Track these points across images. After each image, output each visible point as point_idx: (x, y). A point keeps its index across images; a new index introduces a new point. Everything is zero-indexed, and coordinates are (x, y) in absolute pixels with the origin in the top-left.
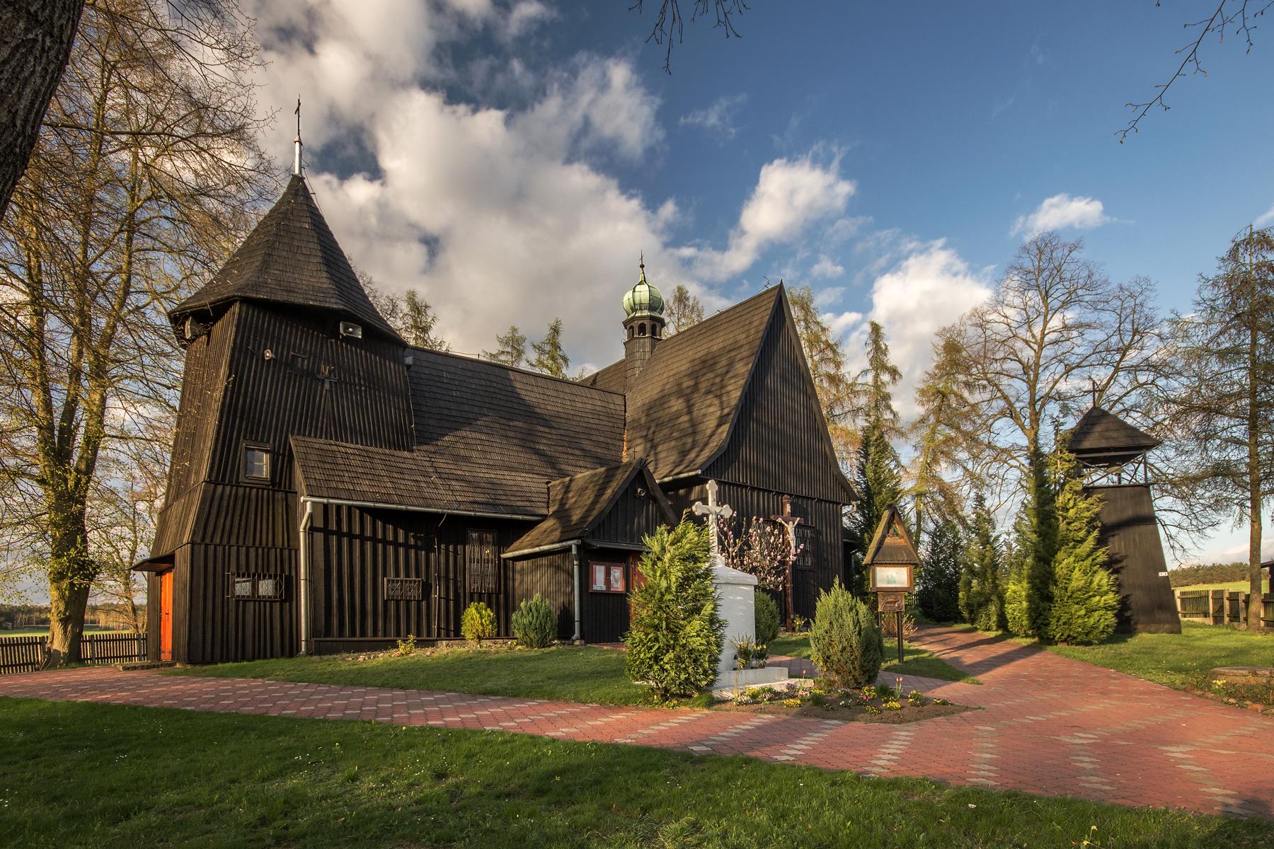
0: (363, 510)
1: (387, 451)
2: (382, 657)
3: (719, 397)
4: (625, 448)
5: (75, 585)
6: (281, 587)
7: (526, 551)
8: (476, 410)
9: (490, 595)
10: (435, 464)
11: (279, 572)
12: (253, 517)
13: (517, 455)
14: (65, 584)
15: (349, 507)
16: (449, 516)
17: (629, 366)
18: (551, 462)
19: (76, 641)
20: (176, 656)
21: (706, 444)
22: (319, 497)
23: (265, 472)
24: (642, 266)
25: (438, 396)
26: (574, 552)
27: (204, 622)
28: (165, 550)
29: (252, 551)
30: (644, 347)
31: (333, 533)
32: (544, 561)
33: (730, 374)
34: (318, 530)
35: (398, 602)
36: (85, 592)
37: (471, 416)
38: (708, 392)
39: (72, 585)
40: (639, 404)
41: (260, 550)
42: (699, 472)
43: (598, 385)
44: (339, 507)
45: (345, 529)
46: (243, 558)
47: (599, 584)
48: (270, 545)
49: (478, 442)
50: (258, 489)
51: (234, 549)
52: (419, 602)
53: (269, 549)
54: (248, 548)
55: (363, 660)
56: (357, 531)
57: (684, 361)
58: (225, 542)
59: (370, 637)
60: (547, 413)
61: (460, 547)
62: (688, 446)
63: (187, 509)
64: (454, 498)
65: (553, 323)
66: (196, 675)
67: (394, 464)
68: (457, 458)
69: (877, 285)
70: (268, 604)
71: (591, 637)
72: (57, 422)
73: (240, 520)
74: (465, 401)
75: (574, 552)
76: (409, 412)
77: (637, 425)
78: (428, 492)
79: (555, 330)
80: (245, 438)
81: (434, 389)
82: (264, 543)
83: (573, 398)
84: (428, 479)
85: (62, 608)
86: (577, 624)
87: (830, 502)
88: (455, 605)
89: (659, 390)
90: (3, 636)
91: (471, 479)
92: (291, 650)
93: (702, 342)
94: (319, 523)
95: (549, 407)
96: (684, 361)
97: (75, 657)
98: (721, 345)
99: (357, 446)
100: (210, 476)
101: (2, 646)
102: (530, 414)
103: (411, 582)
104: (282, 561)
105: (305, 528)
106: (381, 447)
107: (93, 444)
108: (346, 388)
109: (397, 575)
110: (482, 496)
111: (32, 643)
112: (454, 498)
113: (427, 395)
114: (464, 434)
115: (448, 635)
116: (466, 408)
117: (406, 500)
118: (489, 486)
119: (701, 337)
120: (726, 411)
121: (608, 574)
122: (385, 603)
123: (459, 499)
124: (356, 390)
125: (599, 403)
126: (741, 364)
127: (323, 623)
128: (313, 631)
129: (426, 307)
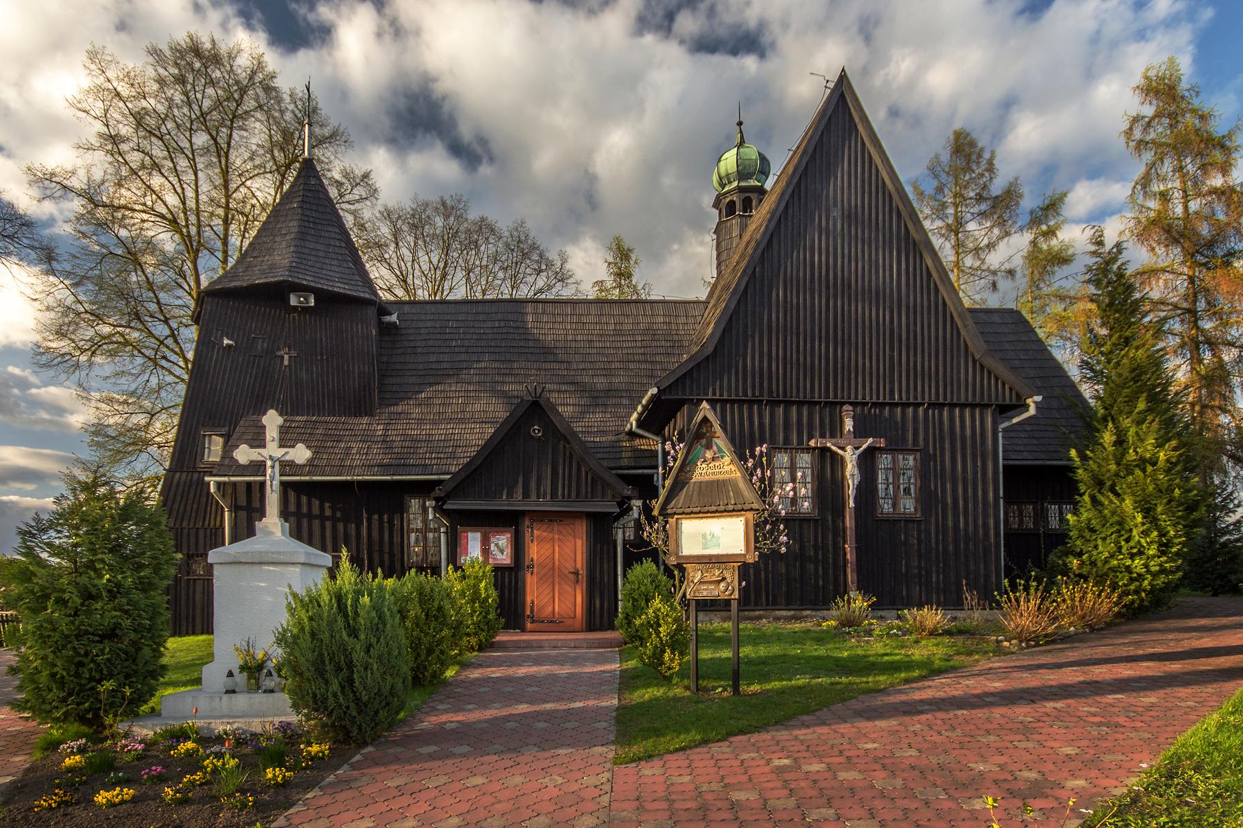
22: (220, 476)
24: (740, 124)
69: (682, 11)
82: (212, 524)
90: (4, 613)
101: (3, 622)
116: (433, 358)
121: (1021, 522)
129: (629, 250)
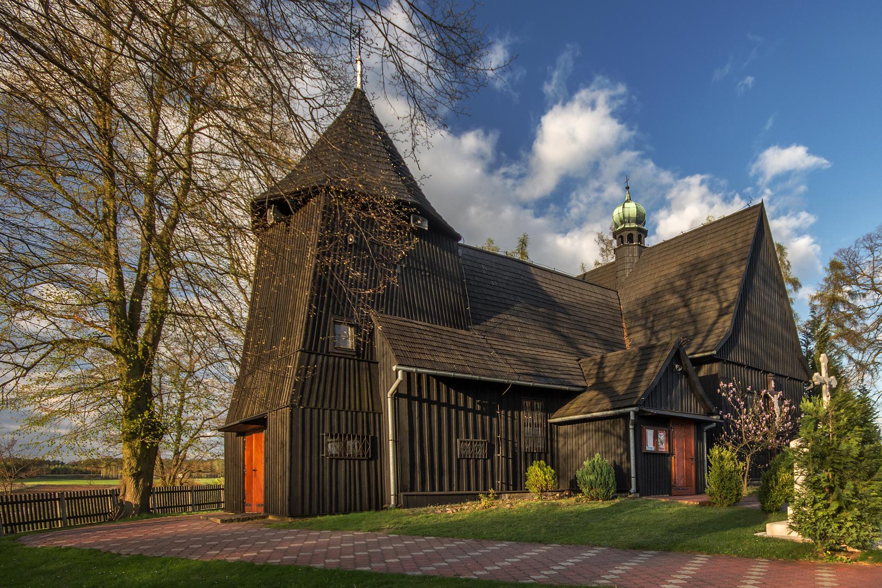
0: (439, 378)
1: (449, 329)
2: (469, 509)
3: (716, 293)
4: (626, 334)
5: (147, 444)
6: (368, 447)
7: (577, 417)
8: (511, 297)
9: (540, 454)
10: (489, 342)
11: (365, 434)
12: (342, 383)
13: (549, 338)
14: (137, 443)
15: (428, 375)
16: (514, 385)
17: (619, 268)
18: (570, 342)
19: (147, 492)
20: (269, 508)
21: (710, 331)
22: (408, 366)
23: (350, 344)
25: (481, 284)
26: (632, 417)
27: (303, 478)
28: (251, 411)
29: (343, 414)
30: (633, 253)
31: (415, 399)
32: (591, 426)
33: (723, 275)
34: (403, 396)
35: (468, 460)
36: (155, 451)
37: (508, 302)
38: (702, 290)
39: (144, 444)
40: (633, 299)
41: (349, 413)
42: (715, 352)
43: (586, 280)
44: (420, 375)
45: (425, 396)
46: (335, 421)
47: (650, 446)
48: (358, 409)
49: (517, 324)
50: (345, 358)
51: (327, 412)
52: (485, 460)
53: (357, 412)
54: (339, 411)
55: (450, 512)
56: (435, 398)
57: (674, 264)
58: (319, 406)
59: (446, 491)
60: (563, 302)
61: (516, 413)
62: (691, 333)
63: (278, 377)
64: (512, 371)
65: (522, 237)
66: (309, 527)
67: (458, 340)
68: (503, 337)
70: (357, 462)
71: (645, 490)
72: (128, 298)
73: (332, 386)
74: (502, 290)
75: (632, 417)
76: (465, 296)
77: (632, 316)
78: (491, 365)
79: (524, 243)
80: (333, 313)
81: (477, 279)
83: (581, 291)
84: (488, 354)
85: (134, 464)
86: (633, 480)
87: (797, 380)
88: (513, 463)
89: (653, 286)
91: (518, 354)
92: (378, 503)
93: (690, 249)
94: (404, 391)
95: (565, 298)
96: (674, 264)
97: (144, 509)
98: (710, 252)
99: (429, 325)
100: (304, 346)
102: (549, 302)
103: (478, 442)
104: (368, 423)
105: (392, 395)
106: (444, 325)
107: (158, 318)
108: (414, 272)
109: (467, 437)
110: (533, 369)
111: (101, 495)
112: (512, 371)
113: (472, 283)
114: (506, 317)
115: (508, 489)
116: (504, 296)
117: (477, 371)
118: (532, 360)
119: (688, 245)
120: (725, 305)
122: (458, 460)
123: (518, 371)
124: (422, 275)
125: (600, 297)
126: (733, 266)
127: (409, 479)
128: (400, 488)
